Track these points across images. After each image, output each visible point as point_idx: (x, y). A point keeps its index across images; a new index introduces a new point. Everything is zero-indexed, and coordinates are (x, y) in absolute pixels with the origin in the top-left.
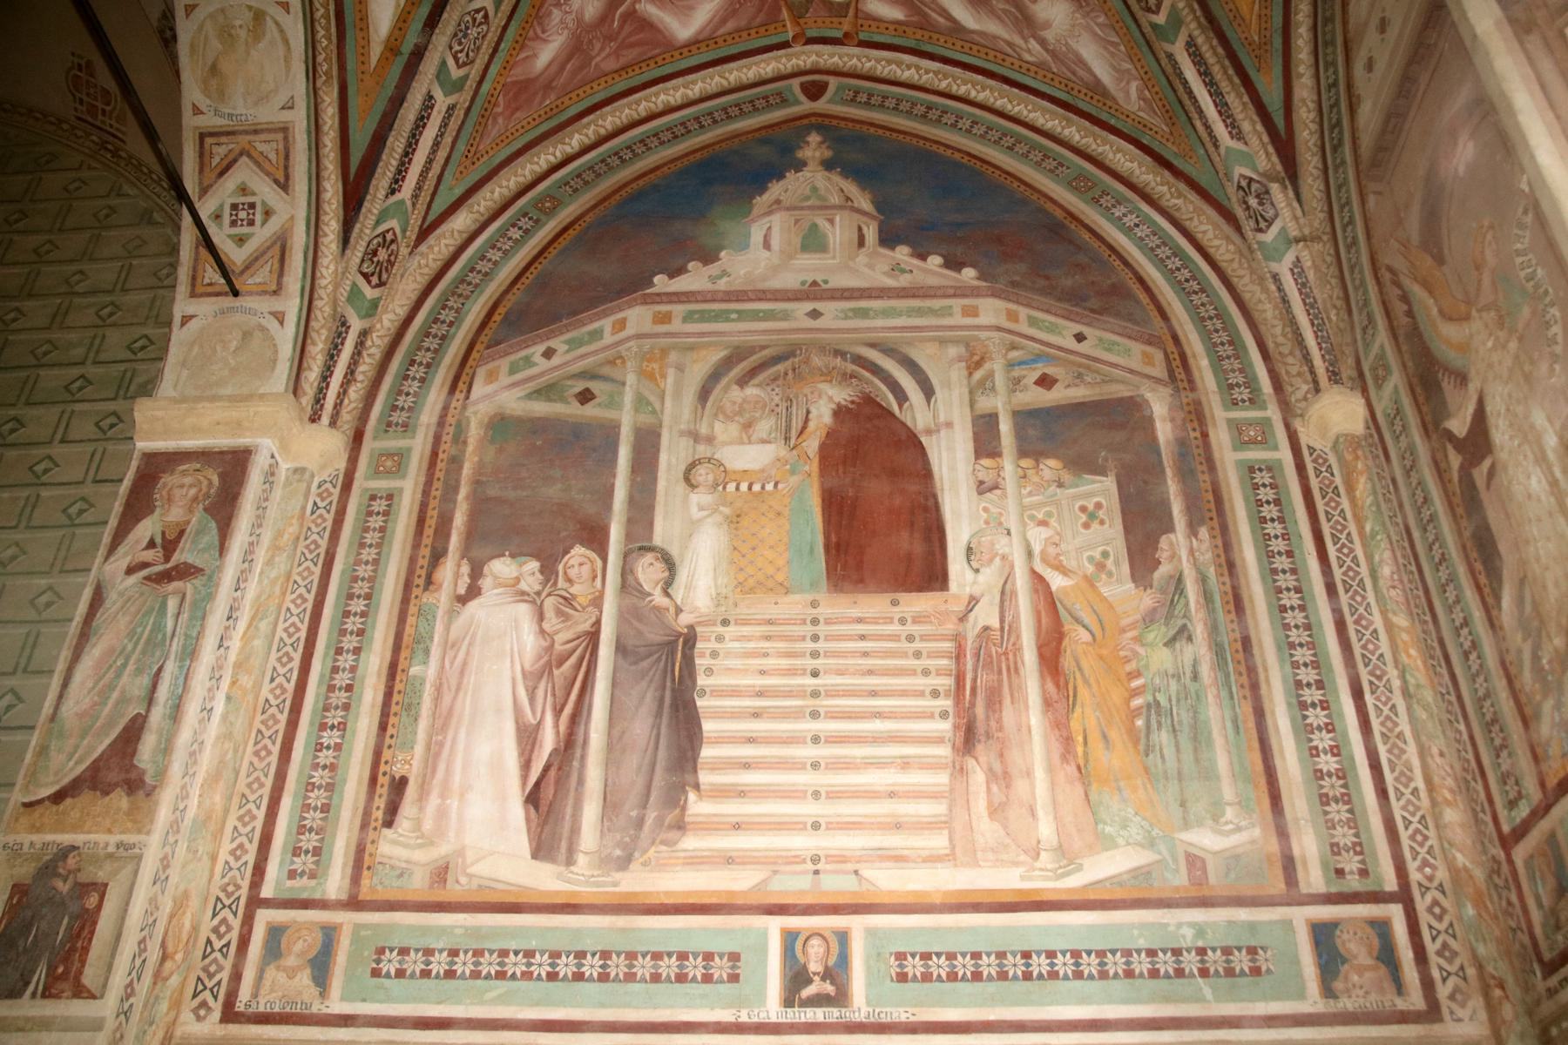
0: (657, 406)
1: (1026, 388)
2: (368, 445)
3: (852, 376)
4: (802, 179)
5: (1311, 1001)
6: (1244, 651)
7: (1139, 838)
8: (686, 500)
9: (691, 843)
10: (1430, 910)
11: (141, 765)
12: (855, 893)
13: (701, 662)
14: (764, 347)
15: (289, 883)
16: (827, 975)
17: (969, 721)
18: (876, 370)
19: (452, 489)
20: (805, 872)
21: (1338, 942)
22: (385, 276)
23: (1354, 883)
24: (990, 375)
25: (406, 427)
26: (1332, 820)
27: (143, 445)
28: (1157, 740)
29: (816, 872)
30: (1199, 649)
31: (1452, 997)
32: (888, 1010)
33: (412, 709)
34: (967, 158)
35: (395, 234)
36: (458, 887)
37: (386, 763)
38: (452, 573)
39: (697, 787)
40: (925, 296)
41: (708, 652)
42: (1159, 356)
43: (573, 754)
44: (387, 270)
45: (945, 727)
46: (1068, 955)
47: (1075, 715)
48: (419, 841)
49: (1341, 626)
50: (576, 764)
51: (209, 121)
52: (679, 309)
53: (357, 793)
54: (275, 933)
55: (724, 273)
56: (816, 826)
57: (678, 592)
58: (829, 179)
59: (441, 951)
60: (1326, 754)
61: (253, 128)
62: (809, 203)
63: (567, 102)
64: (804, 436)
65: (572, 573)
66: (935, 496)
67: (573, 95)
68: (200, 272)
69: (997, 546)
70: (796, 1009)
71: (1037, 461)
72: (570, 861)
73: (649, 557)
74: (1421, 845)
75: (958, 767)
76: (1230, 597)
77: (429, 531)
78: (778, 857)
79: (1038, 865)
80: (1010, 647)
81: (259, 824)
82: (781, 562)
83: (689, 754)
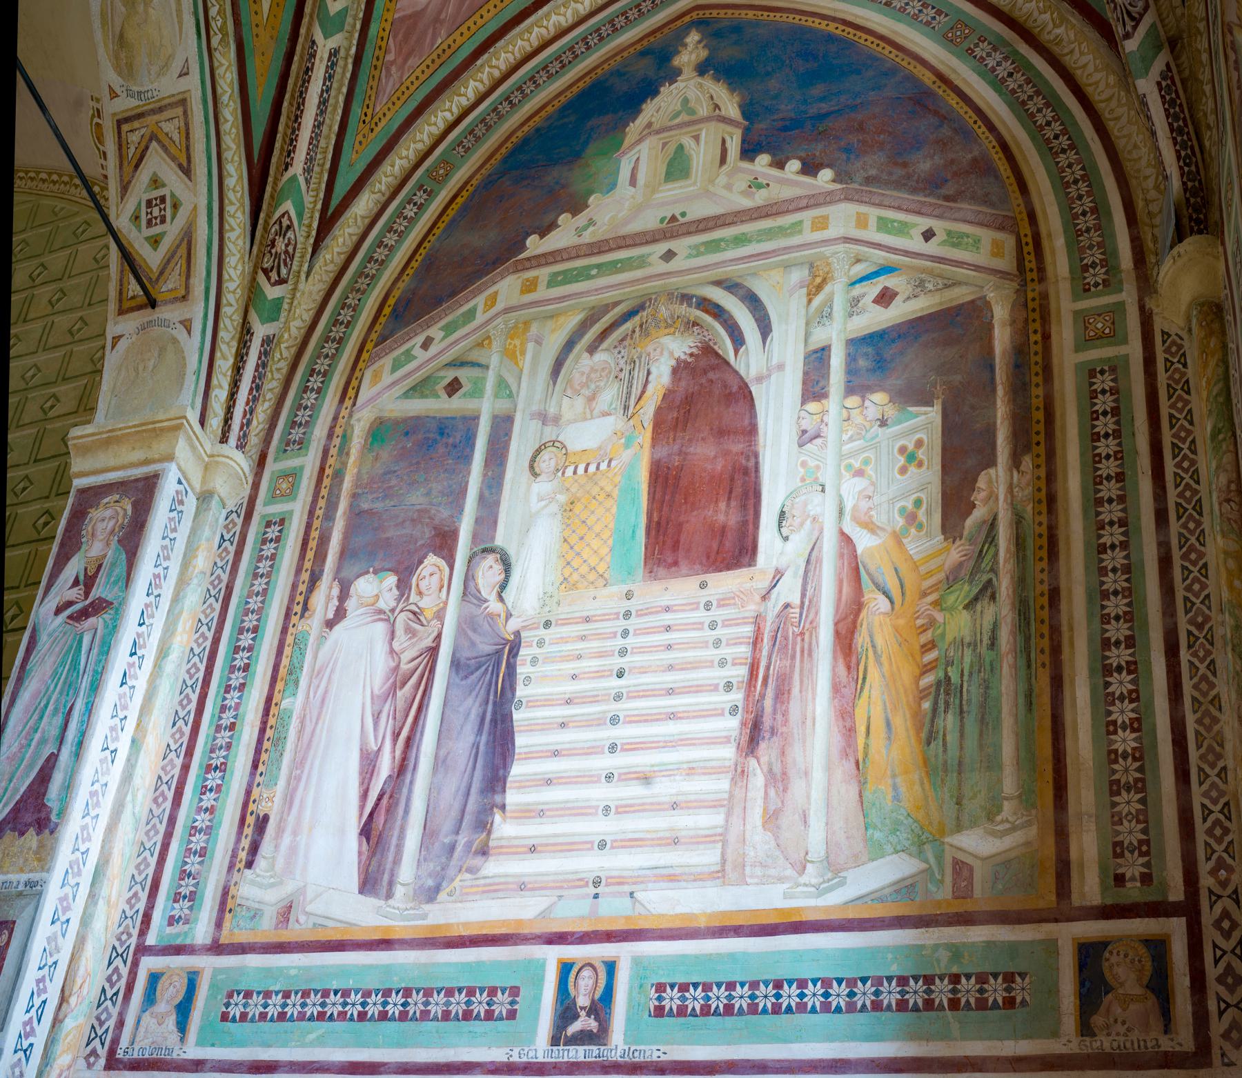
0: (514, 388)
1: (863, 311)
2: (271, 467)
3: (695, 324)
4: (675, 92)
5: (1064, 1040)
6: (1051, 606)
7: (907, 843)
8: (529, 486)
9: (493, 868)
10: (1217, 924)
11: (49, 804)
12: (628, 918)
13: (522, 670)
14: (616, 304)
15: (169, 930)
16: (593, 1010)
17: (756, 717)
18: (717, 312)
19: (332, 506)
20: (585, 897)
21: (1105, 965)
22: (284, 271)
23: (1133, 892)
24: (829, 302)
25: (302, 444)
26: (1120, 813)
27: (78, 483)
28: (942, 724)
29: (596, 896)
30: (1003, 610)
31: (1226, 1036)
32: (642, 1047)
33: (279, 742)
34: (841, 27)
35: (290, 219)
36: (297, 926)
37: (254, 801)
38: (323, 599)
39: (503, 807)
40: (778, 214)
41: (529, 658)
42: (1009, 241)
43: (403, 781)
44: (286, 264)
45: (732, 724)
46: (819, 984)
47: (862, 700)
48: (272, 880)
49: (1165, 563)
50: (405, 790)
51: (125, 104)
52: (544, 273)
53: (229, 834)
54: (154, 978)
55: (591, 222)
56: (602, 845)
57: (509, 595)
58: (701, 85)
59: (277, 993)
60: (1124, 730)
61: (157, 105)
62: (677, 121)
63: (459, 40)
64: (642, 402)
65: (423, 585)
66: (756, 456)
67: (463, 29)
68: (125, 284)
69: (809, 507)
70: (561, 1047)
71: (863, 399)
72: (389, 895)
73: (490, 559)
74: (1219, 840)
75: (739, 770)
76: (1044, 541)
77: (310, 555)
78: (565, 881)
79: (804, 879)
80: (807, 626)
81: (151, 871)
82: (605, 550)
83: (501, 772)
